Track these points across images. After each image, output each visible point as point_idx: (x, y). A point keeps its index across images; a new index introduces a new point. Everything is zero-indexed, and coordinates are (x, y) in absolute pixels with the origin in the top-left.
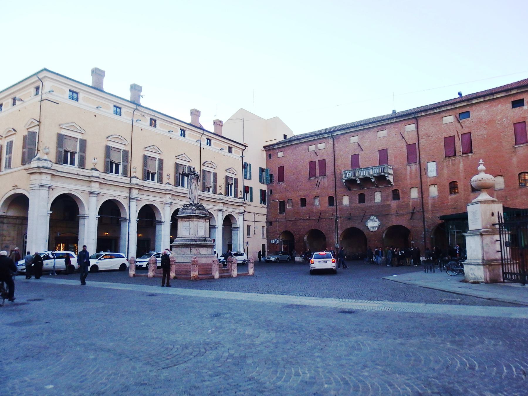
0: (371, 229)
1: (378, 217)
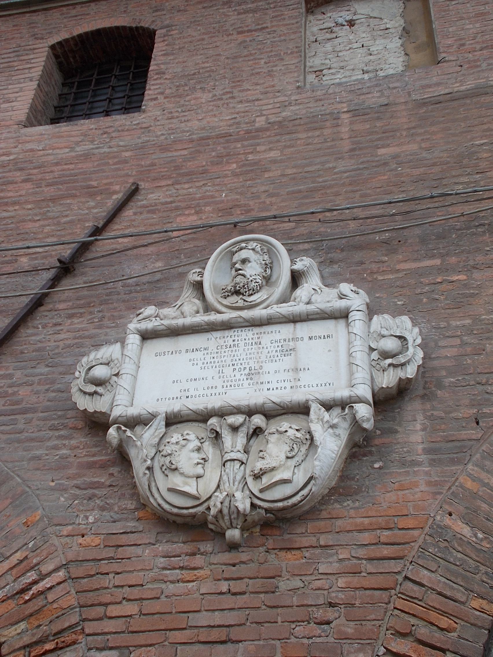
0: (194, 474)
1: (343, 248)
